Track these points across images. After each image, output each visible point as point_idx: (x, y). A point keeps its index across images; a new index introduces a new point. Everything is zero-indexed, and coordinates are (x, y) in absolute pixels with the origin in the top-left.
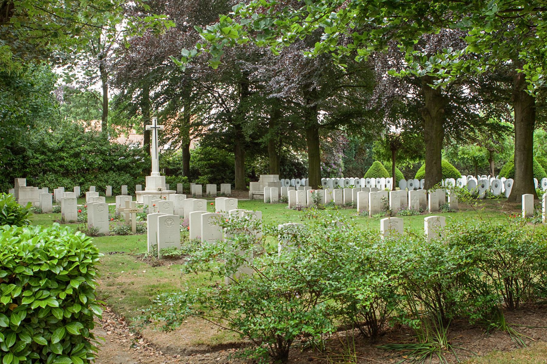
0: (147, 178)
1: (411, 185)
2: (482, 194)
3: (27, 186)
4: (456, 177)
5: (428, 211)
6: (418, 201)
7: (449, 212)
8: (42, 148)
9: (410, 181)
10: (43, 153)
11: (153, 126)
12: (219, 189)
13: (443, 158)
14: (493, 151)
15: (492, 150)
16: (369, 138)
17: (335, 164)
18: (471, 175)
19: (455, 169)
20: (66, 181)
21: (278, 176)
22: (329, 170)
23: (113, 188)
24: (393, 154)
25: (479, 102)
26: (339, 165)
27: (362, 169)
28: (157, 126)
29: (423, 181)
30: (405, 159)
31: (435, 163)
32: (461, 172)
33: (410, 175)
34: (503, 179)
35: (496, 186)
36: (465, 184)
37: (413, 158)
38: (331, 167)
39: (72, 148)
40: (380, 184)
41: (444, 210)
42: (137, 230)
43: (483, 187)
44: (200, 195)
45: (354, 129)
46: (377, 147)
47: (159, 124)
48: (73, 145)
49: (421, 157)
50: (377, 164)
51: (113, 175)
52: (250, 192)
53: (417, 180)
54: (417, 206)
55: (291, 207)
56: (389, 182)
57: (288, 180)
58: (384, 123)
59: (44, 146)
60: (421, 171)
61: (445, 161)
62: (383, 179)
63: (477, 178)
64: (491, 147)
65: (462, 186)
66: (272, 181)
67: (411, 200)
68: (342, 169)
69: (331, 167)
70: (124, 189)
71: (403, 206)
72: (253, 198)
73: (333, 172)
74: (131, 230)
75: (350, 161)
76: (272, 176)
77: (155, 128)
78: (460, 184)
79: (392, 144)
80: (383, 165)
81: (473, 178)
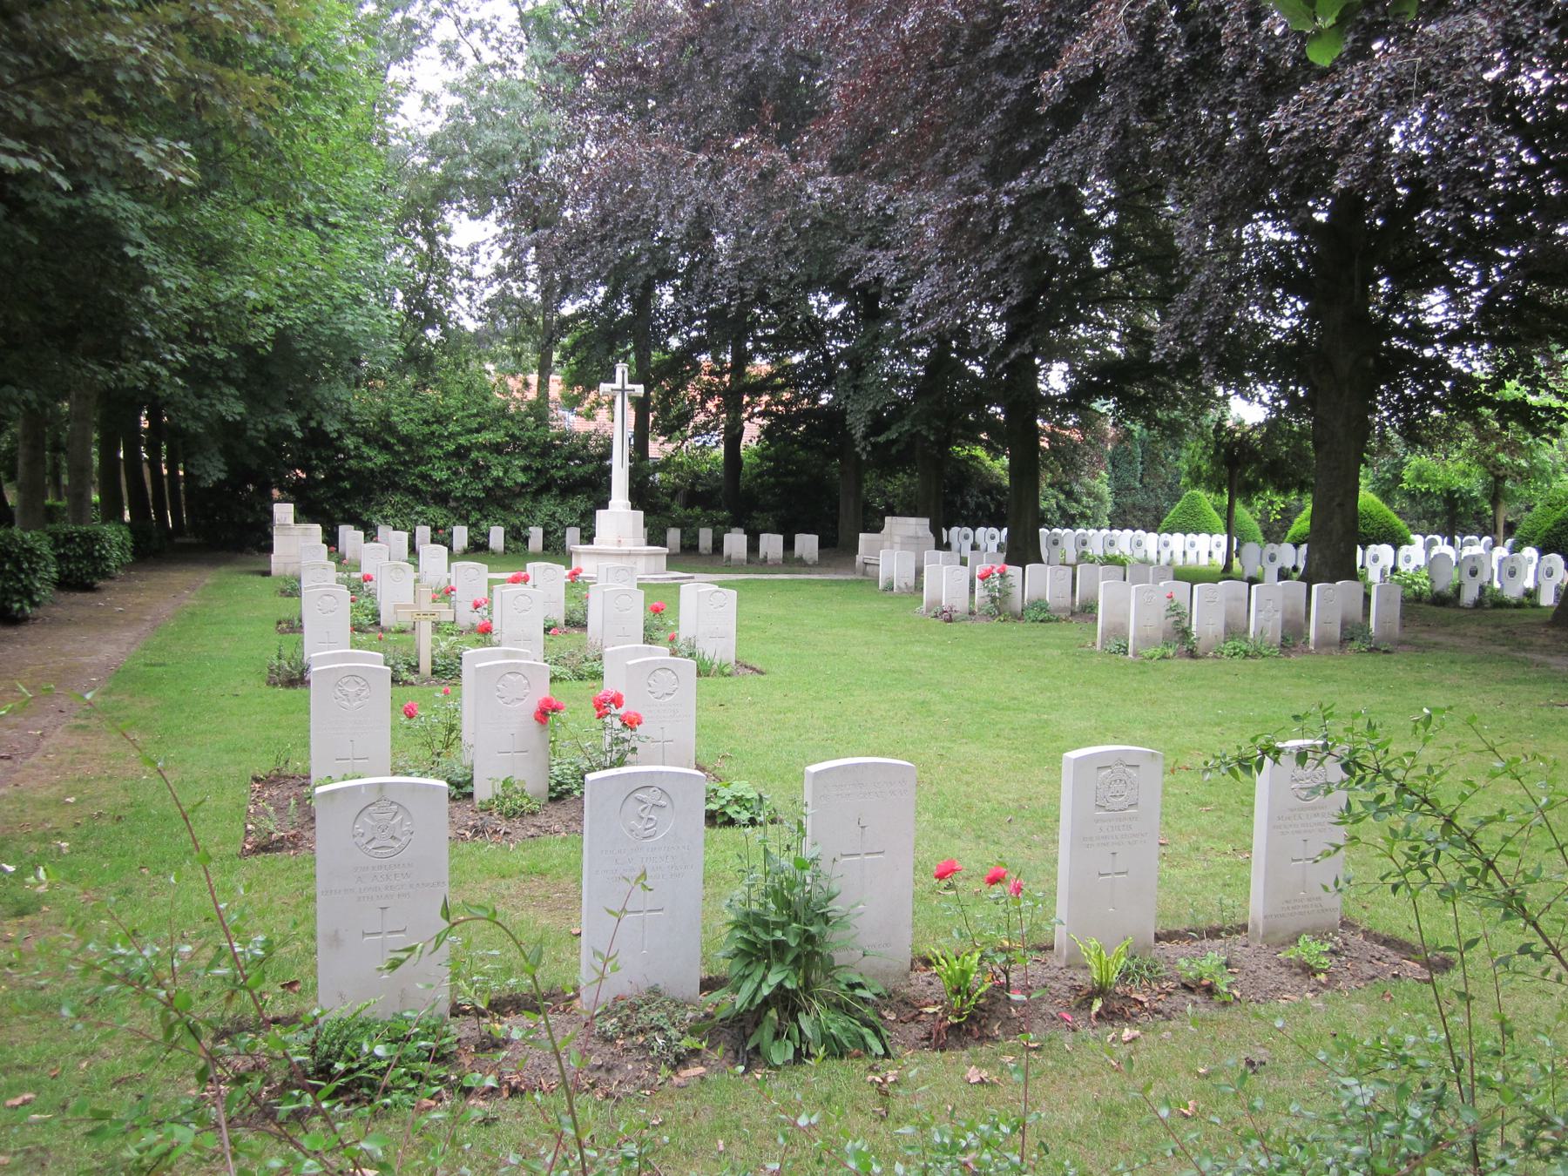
0: (600, 514)
1: (1272, 558)
2: (1469, 595)
3: (296, 521)
4: (1397, 541)
5: (1306, 643)
6: (1279, 616)
7: (1370, 650)
8: (382, 434)
9: (1271, 548)
10: (386, 447)
11: (618, 385)
12: (789, 545)
13: (1361, 493)
14: (1504, 478)
15: (1501, 473)
16: (1173, 431)
17: (1089, 495)
18: (1437, 533)
19: (1396, 519)
20: (434, 512)
21: (926, 521)
22: (1074, 509)
23: (546, 534)
24: (1231, 474)
25: (1477, 341)
26: (1098, 498)
27: (1157, 508)
28: (628, 386)
29: (1304, 548)
30: (1263, 489)
31: (1340, 505)
32: (1410, 526)
33: (1483, 386)
34: (1530, 552)
35: (1512, 574)
36: (1422, 563)
37: (1283, 489)
38: (1078, 501)
39: (451, 436)
40: (1196, 549)
41: (1355, 645)
42: (434, 672)
43: (1474, 573)
44: (741, 561)
45: (1131, 406)
46: (1191, 454)
47: (630, 382)
48: (452, 427)
49: (1302, 487)
50: (1194, 498)
51: (548, 505)
52: (859, 558)
53: (1291, 547)
54: (1274, 632)
55: (928, 610)
56: (1218, 545)
57: (968, 530)
58: (220, 46)
59: (390, 428)
60: (1301, 524)
61: (1367, 498)
62: (1204, 537)
63: (1452, 543)
64: (1498, 466)
65: (1412, 566)
66: (911, 533)
67: (1258, 611)
68: (1109, 507)
69: (1078, 501)
70: (536, 535)
71: (1234, 630)
72: (865, 573)
73: (1083, 516)
74: (414, 669)
75: (1129, 488)
76: (912, 520)
77: (623, 391)
78: (1408, 559)
79: (1229, 452)
80: (1206, 500)
81: (1442, 547)
